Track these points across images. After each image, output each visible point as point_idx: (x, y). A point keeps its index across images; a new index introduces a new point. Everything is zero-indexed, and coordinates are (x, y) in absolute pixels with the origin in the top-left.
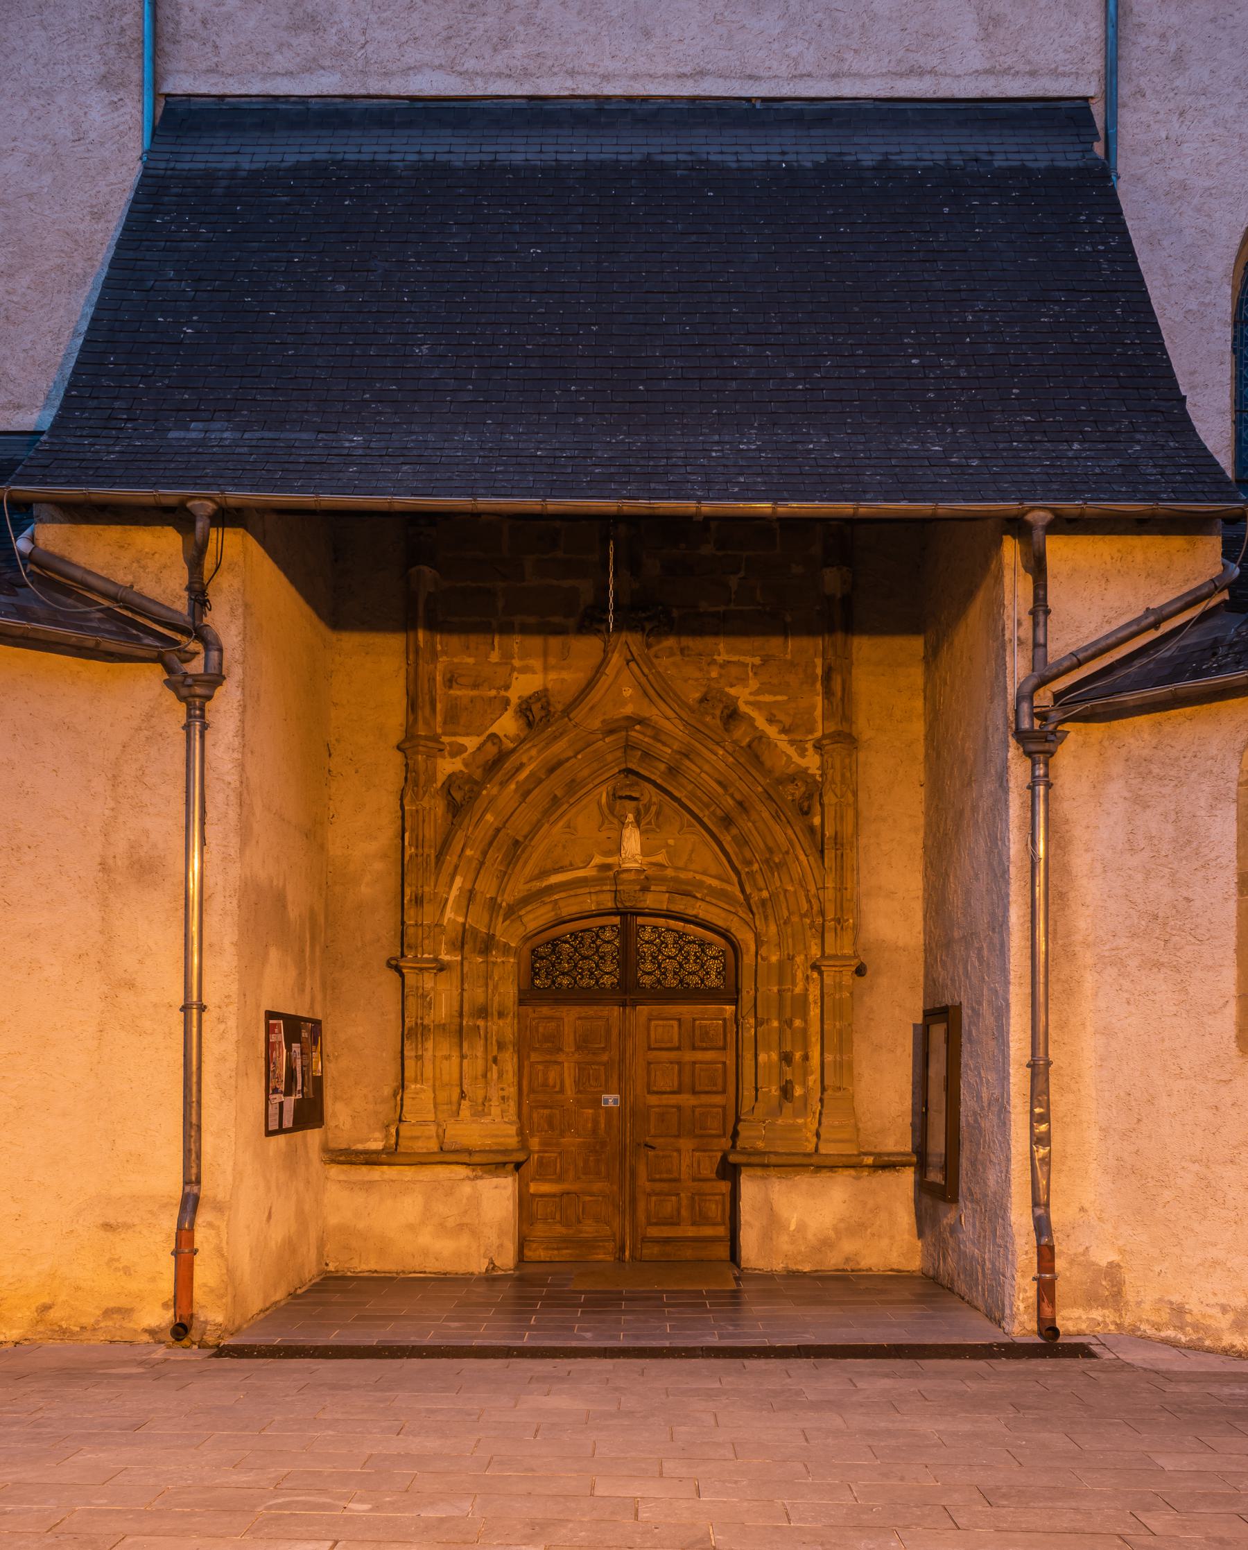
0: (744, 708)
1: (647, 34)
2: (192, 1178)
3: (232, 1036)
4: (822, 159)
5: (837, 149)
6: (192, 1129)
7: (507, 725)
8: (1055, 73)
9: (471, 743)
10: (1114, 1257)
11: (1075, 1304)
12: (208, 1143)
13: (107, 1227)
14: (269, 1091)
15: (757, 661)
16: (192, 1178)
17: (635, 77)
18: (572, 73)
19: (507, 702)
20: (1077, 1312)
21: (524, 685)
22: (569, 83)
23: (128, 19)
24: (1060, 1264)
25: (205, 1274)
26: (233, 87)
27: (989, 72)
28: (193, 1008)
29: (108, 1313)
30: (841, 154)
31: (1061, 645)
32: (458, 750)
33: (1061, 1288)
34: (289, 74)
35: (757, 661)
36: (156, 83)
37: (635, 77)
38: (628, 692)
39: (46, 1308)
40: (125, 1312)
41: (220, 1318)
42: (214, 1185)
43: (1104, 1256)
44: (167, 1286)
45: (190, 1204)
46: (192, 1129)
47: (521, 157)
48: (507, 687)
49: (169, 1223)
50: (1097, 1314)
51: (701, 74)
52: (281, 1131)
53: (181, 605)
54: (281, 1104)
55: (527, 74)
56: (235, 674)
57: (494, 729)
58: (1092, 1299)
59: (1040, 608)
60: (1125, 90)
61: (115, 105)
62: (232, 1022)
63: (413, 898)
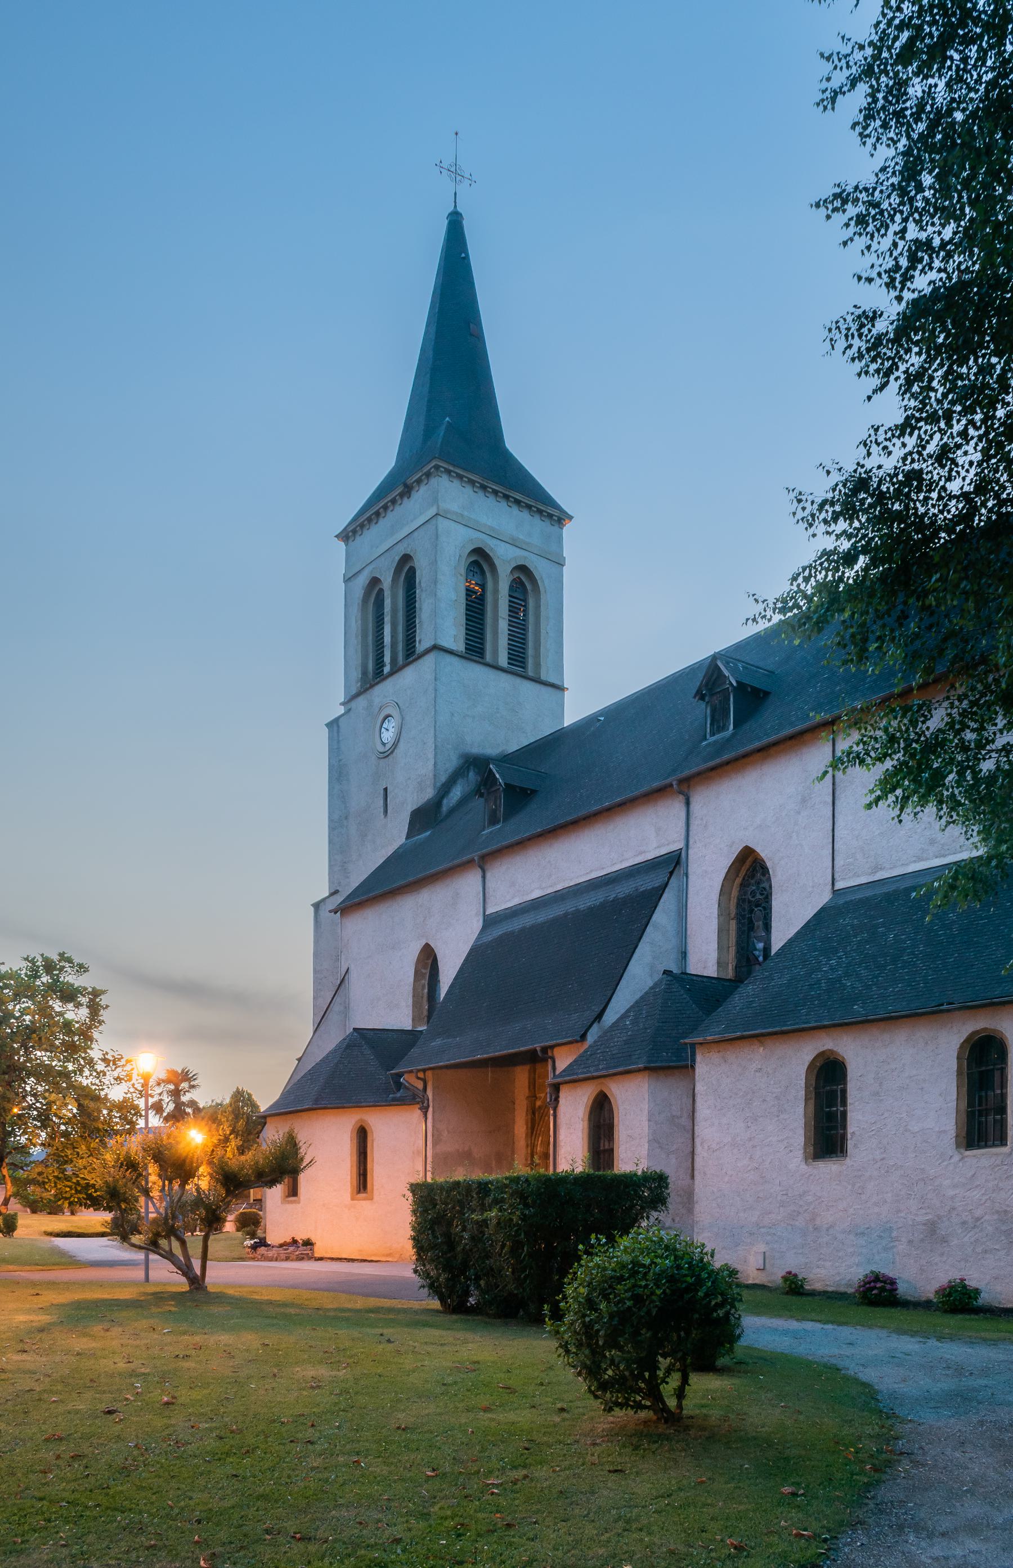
1: (580, 862)
4: (602, 900)
27: (658, 847)
37: (577, 877)
51: (591, 871)
60: (691, 843)
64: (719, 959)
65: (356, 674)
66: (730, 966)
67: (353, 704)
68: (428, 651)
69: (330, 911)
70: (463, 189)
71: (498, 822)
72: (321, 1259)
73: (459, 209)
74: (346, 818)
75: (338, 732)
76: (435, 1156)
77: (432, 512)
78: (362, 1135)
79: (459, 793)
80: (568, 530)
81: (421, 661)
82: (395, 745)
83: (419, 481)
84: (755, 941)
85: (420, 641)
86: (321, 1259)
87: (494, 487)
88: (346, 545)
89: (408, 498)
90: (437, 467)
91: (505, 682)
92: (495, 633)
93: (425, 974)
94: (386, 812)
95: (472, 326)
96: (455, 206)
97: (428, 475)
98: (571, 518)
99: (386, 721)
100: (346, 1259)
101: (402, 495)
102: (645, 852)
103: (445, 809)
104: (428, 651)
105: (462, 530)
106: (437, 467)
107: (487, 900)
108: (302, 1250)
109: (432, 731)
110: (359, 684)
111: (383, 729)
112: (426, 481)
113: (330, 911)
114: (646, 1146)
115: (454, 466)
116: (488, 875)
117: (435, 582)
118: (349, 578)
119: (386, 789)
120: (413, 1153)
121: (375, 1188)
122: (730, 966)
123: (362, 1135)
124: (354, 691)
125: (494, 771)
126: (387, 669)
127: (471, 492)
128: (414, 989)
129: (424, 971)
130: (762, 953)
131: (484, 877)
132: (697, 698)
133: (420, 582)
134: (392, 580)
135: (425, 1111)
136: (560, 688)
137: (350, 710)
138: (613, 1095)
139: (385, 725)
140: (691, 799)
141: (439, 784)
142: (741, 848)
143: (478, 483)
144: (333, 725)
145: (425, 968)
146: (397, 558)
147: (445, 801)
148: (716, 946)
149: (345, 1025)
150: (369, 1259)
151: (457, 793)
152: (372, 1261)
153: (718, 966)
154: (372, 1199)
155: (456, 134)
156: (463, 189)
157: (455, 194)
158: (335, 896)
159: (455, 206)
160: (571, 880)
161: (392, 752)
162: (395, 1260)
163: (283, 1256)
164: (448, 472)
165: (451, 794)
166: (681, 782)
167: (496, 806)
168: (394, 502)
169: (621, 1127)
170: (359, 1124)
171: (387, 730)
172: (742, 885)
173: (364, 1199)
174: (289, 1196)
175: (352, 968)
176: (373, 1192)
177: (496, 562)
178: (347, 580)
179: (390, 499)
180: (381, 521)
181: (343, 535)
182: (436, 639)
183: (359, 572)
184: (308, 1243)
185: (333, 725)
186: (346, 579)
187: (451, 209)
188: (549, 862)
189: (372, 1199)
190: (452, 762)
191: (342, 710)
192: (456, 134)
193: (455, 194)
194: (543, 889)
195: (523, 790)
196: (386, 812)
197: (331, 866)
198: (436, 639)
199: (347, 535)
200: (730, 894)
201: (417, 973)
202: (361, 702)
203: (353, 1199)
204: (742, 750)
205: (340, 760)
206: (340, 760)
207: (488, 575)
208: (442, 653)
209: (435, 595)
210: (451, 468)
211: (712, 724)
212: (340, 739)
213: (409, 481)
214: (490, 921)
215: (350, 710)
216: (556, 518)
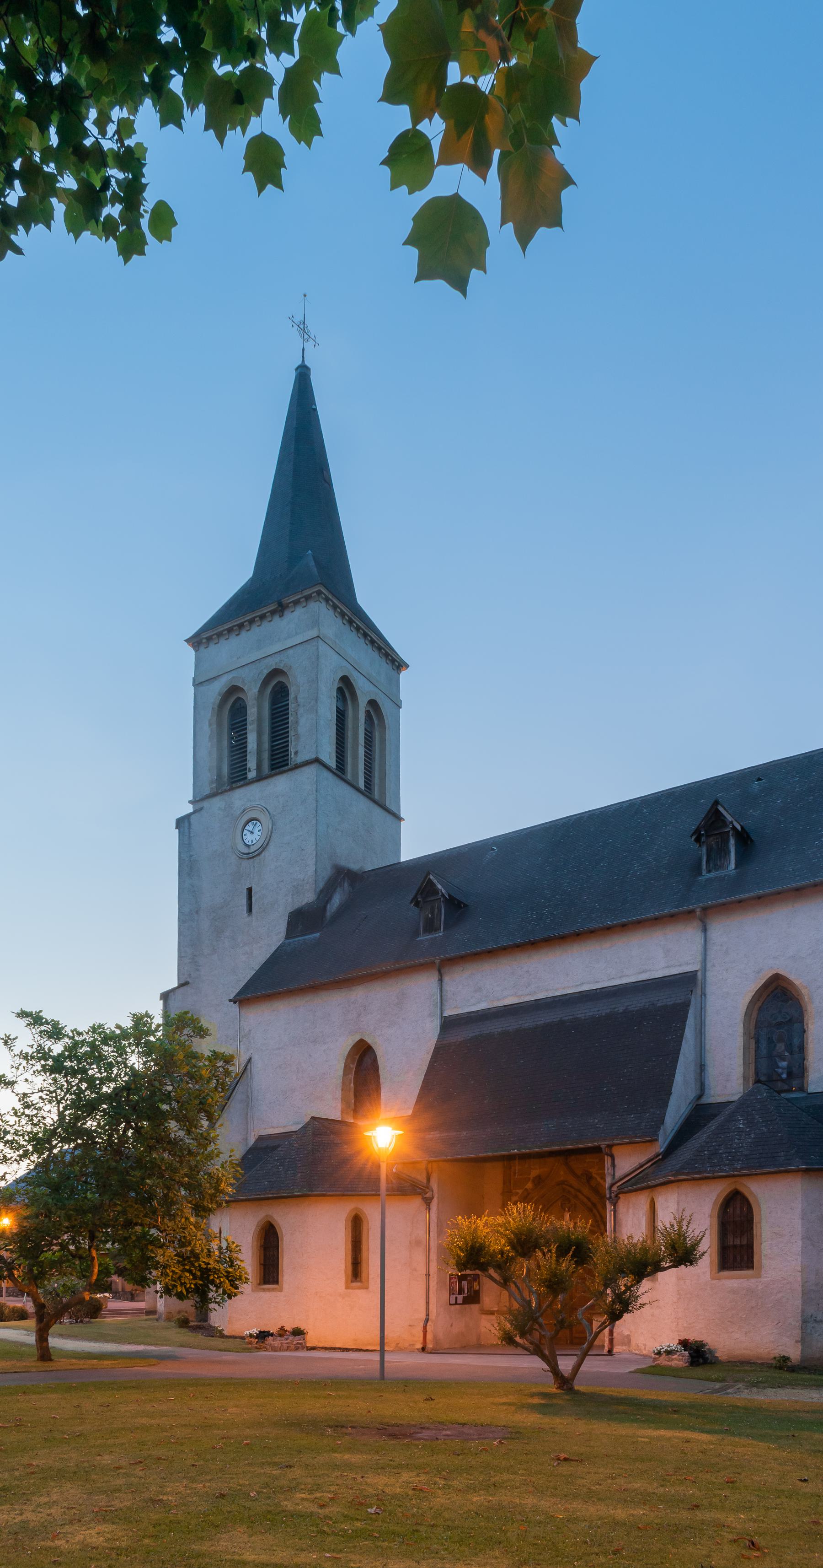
0: (594, 1175)
1: (567, 975)
2: (428, 1315)
3: (436, 1281)
4: (608, 1011)
5: (613, 1006)
6: (428, 1303)
7: (529, 1185)
8: (687, 964)
9: (520, 1191)
10: (629, 1333)
11: (619, 1345)
12: (431, 1306)
13: (410, 1326)
14: (451, 1292)
15: (597, 1160)
16: (428, 1315)
17: (564, 988)
18: (547, 991)
19: (529, 1179)
20: (619, 1347)
21: (534, 1173)
22: (546, 994)
23: (435, 997)
24: (615, 1334)
25: (429, 1337)
26: (460, 1011)
27: (667, 967)
28: (428, 1275)
29: (410, 1345)
30: (615, 1008)
31: (619, 1173)
32: (517, 1194)
33: (615, 1341)
34: (474, 1005)
35: (597, 1160)
36: (442, 1014)
37: (564, 988)
38: (562, 1173)
39: (398, 1344)
40: (413, 1345)
41: (431, 1346)
42: (433, 1316)
43: (626, 1333)
44: (421, 1339)
45: (427, 1320)
46: (428, 1303)
47: (527, 1025)
48: (530, 1174)
49: (422, 1324)
50: (624, 1348)
51: (582, 984)
52: (456, 1304)
53: (425, 1181)
54: (456, 1298)
55: (535, 993)
56: (436, 1196)
57: (526, 1187)
58: (623, 1344)
59: (613, 1165)
60: (709, 965)
61: (432, 1021)
62: (436, 1278)
63: (95, 1367)
64: (744, 1073)
65: (208, 776)
66: (751, 1080)
67: (206, 804)
68: (307, 763)
69: (230, 1001)
70: (309, 345)
71: (437, 930)
72: (313, 1348)
73: (307, 363)
74: (197, 912)
75: (189, 828)
76: (440, 1247)
77: (313, 633)
78: (357, 1224)
79: (338, 901)
80: (404, 675)
81: (298, 771)
82: (264, 848)
83: (296, 603)
84: (777, 1059)
85: (296, 753)
86: (313, 1348)
87: (359, 624)
88: (196, 651)
89: (280, 617)
90: (319, 593)
91: (361, 804)
92: (355, 757)
93: (352, 1069)
94: (250, 910)
95: (325, 472)
96: (303, 361)
97: (308, 598)
98: (407, 666)
99: (250, 824)
100: (340, 1348)
101: (273, 613)
102: (650, 970)
103: (329, 914)
104: (307, 763)
105: (336, 656)
106: (319, 593)
107: (444, 1002)
108: (297, 1340)
109: (313, 839)
110: (214, 785)
111: (245, 832)
112: (304, 604)
113: (230, 1001)
114: (800, 1243)
115: (333, 595)
116: (446, 979)
117: (316, 700)
118: (201, 683)
119: (250, 890)
120: (410, 1242)
121: (371, 1277)
122: (751, 1080)
123: (357, 1224)
124: (207, 791)
125: (435, 881)
126: (252, 775)
127: (341, 622)
128: (343, 1083)
129: (351, 1066)
130: (785, 1071)
131: (441, 980)
132: (694, 838)
133: (296, 698)
134: (259, 691)
135: (428, 1202)
136: (399, 819)
137: (201, 809)
138: (752, 1193)
139: (247, 827)
140: (708, 927)
141: (318, 890)
142: (770, 975)
143: (348, 616)
144: (182, 823)
145: (353, 1064)
146: (266, 672)
147: (328, 907)
148: (742, 1061)
149: (247, 1114)
150: (365, 1348)
151: (337, 901)
152: (367, 1350)
153: (744, 1080)
154: (367, 1288)
155: (305, 296)
156: (309, 345)
157: (303, 349)
158: (185, 988)
159: (303, 361)
160: (556, 990)
161: (259, 855)
162: (392, 1349)
163: (285, 1346)
164: (327, 600)
165: (333, 901)
166: (705, 910)
167: (433, 913)
168: (262, 617)
169: (764, 1224)
170: (353, 1214)
171: (252, 833)
172: (760, 1009)
173: (359, 1288)
174: (260, 1284)
175: (256, 1057)
176: (368, 1281)
177: (358, 692)
178: (197, 684)
179: (259, 614)
180: (244, 633)
181: (195, 640)
182: (317, 753)
183: (215, 678)
184: (298, 1332)
185: (182, 823)
186: (197, 683)
187: (300, 362)
188: (528, 972)
189: (367, 1288)
190: (326, 873)
191: (190, 809)
192: (305, 296)
193: (303, 349)
194: (519, 996)
195: (460, 902)
196: (250, 910)
197: (180, 958)
198: (317, 753)
199: (198, 641)
200: (751, 1015)
201: (346, 1067)
202: (218, 803)
203: (347, 1288)
204: (780, 888)
205: (191, 856)
206: (191, 856)
207: (349, 702)
208: (321, 767)
209: (317, 712)
210: (330, 597)
211: (708, 862)
212: (192, 835)
213: (285, 601)
214: (448, 1024)
215: (201, 809)
216: (397, 664)
